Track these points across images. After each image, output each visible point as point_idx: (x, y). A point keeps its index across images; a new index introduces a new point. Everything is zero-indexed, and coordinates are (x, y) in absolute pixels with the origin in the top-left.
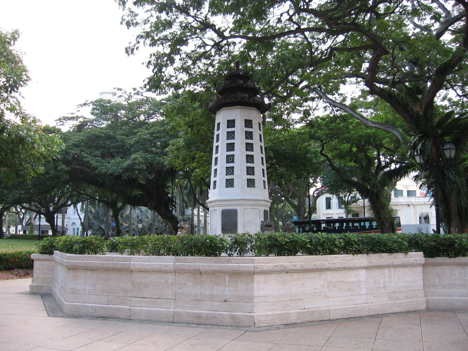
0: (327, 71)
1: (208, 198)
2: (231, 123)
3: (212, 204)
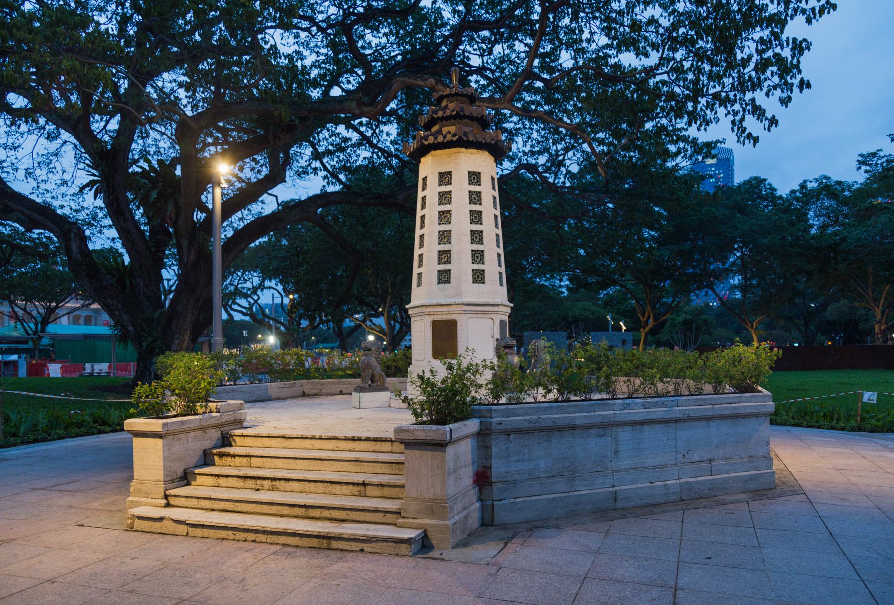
1: (409, 302)
2: (445, 177)
3: (416, 311)
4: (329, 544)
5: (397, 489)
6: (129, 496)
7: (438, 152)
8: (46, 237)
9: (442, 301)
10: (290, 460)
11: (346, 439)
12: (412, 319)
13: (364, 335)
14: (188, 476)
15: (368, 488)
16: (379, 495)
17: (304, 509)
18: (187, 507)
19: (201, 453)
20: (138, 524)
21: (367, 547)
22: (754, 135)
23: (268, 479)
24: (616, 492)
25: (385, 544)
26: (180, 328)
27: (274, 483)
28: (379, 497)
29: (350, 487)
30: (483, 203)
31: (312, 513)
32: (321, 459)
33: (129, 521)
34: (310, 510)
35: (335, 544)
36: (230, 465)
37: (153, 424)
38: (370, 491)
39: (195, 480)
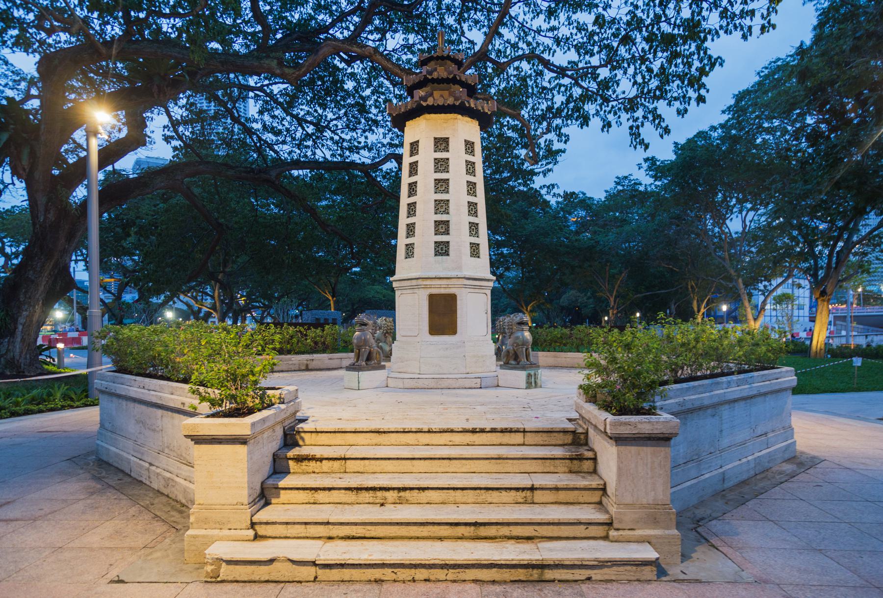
4: (542, 574)
5: (576, 492)
6: (187, 530)
7: (433, 115)
8: (396, 96)
9: (442, 275)
10: (404, 461)
11: (465, 431)
12: (397, 293)
13: (725, 300)
14: (266, 493)
15: (537, 493)
16: (552, 501)
17: (473, 528)
18: (286, 538)
19: (270, 458)
20: (226, 572)
21: (596, 574)
22: (646, 141)
23: (394, 489)
24: (723, 473)
25: (621, 569)
26: (30, 298)
27: (402, 494)
28: (552, 503)
29: (513, 493)
30: (476, 174)
31: (483, 531)
32: (450, 459)
33: (209, 568)
34: (482, 528)
35: (549, 574)
36: (314, 472)
37: (234, 425)
38: (539, 496)
39: (278, 496)
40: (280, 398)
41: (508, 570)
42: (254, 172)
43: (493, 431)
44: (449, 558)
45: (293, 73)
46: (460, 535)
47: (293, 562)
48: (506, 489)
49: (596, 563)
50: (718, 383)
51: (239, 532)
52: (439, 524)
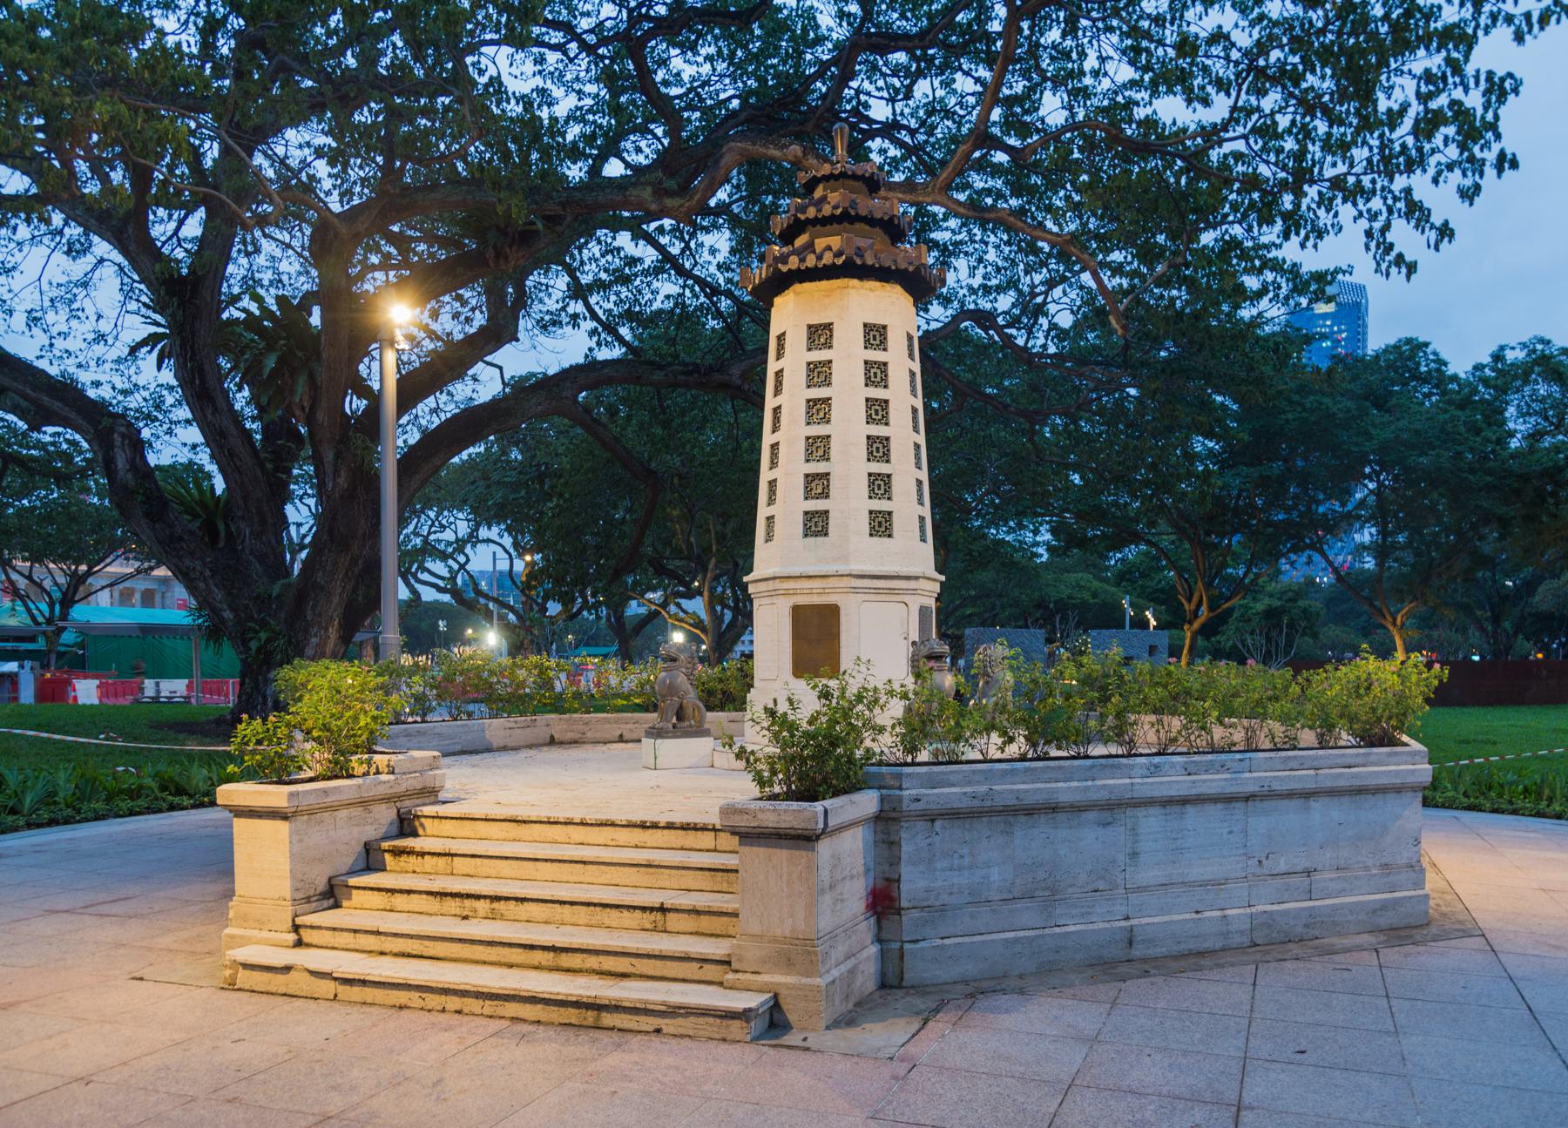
0: (433, 125)
1: (750, 570)
2: (820, 334)
3: (762, 587)
4: (598, 1018)
7: (807, 285)
10: (525, 863)
11: (631, 825)
12: (756, 603)
14: (337, 892)
15: (670, 916)
17: (552, 954)
18: (333, 948)
20: (244, 978)
21: (668, 1025)
22: (1408, 258)
23: (485, 897)
24: (1131, 929)
25: (701, 1020)
27: (495, 905)
28: (691, 933)
29: (638, 914)
31: (567, 960)
32: (584, 863)
35: (608, 1019)
36: (414, 872)
37: (269, 793)
38: (673, 921)
39: (349, 898)
40: (388, 766)
41: (556, 1008)
42: (699, 372)
43: (670, 826)
44: (483, 983)
45: (682, 206)
46: (537, 964)
47: (312, 973)
48: (629, 907)
49: (663, 1008)
50: (1119, 767)
51: (278, 935)
52: (510, 945)
